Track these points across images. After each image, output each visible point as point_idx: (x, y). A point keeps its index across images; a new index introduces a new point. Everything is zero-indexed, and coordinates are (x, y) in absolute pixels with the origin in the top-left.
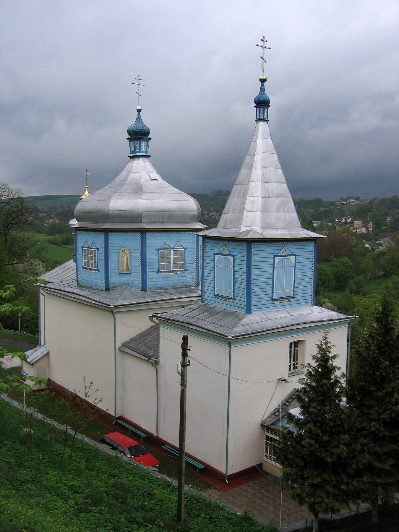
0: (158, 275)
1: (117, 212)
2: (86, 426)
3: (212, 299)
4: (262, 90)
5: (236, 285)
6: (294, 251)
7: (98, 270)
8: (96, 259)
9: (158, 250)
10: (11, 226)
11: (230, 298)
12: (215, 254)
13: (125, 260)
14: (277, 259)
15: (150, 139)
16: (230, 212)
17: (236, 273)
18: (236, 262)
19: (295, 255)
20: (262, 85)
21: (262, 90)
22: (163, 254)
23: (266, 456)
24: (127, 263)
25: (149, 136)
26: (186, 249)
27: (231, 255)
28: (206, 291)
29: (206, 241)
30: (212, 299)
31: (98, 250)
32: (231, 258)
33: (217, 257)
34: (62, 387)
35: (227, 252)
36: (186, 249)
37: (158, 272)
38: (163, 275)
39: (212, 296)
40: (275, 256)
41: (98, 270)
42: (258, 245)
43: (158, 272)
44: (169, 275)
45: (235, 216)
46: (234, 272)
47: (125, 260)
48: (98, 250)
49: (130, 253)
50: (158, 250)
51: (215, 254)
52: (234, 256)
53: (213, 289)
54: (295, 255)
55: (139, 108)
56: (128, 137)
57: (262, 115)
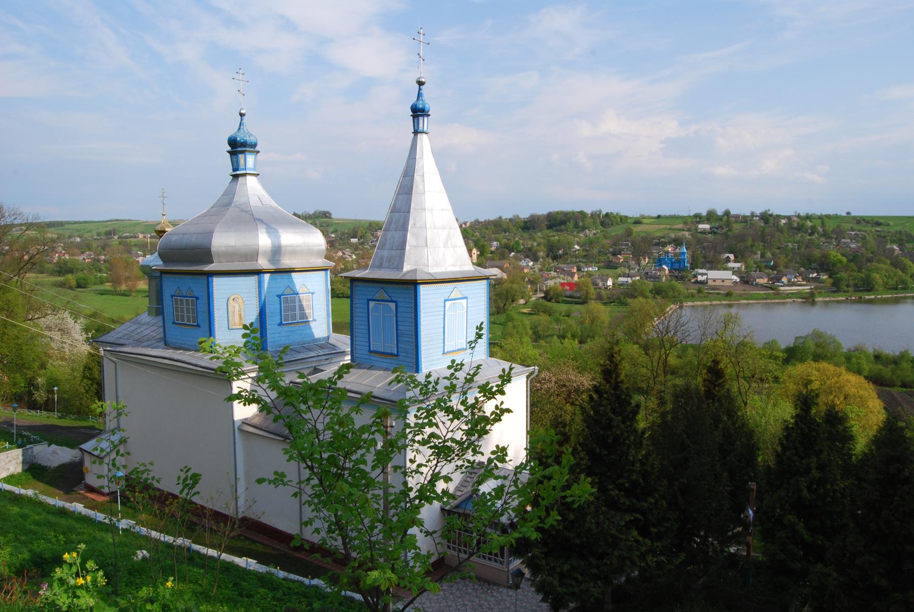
0: (280, 328)
1: (223, 249)
2: (66, 556)
3: (367, 357)
4: (419, 95)
5: (400, 339)
6: (465, 294)
7: (198, 326)
8: (195, 311)
9: (279, 296)
10: (29, 266)
11: (392, 354)
12: (369, 300)
13: (237, 311)
14: (448, 304)
15: (258, 152)
16: (387, 246)
17: (400, 323)
18: (400, 310)
19: (466, 298)
20: (420, 89)
21: (419, 95)
22: (286, 301)
23: (449, 547)
24: (240, 315)
25: (257, 149)
26: (313, 293)
27: (392, 301)
28: (358, 347)
29: (356, 283)
30: (367, 357)
31: (197, 298)
32: (393, 305)
33: (372, 304)
34: (528, 433)
35: (387, 297)
36: (313, 293)
37: (281, 324)
38: (286, 328)
39: (367, 353)
40: (445, 301)
41: (198, 326)
42: (360, 284)
43: (281, 324)
44: (293, 327)
45: (394, 252)
46: (397, 321)
47: (237, 311)
48: (197, 298)
49: (244, 301)
50: (279, 296)
51: (369, 300)
52: (396, 302)
53: (367, 344)
54: (466, 298)
55: (243, 112)
56: (229, 148)
57: (421, 126)
